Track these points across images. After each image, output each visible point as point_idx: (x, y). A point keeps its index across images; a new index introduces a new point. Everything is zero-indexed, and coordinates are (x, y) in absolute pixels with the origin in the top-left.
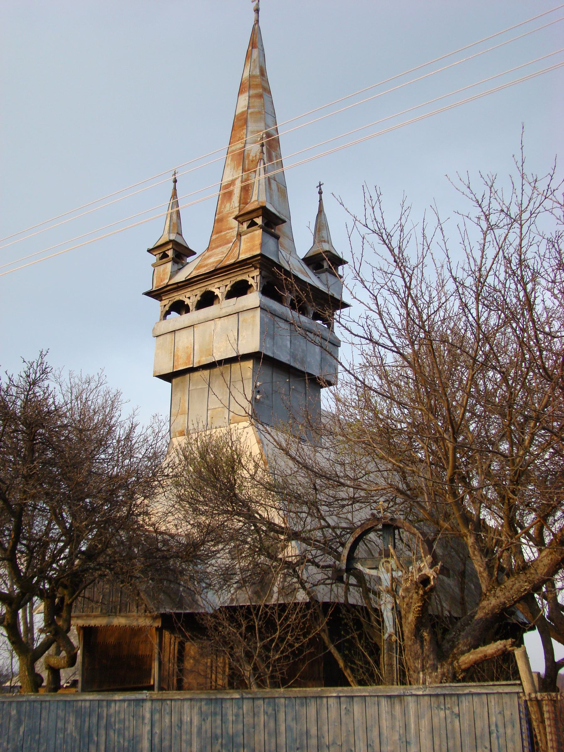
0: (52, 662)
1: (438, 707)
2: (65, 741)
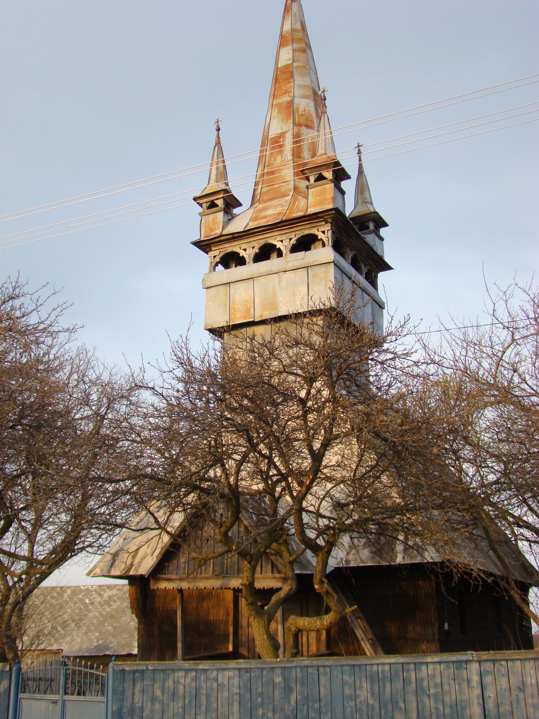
0: (301, 624)
2: (357, 710)
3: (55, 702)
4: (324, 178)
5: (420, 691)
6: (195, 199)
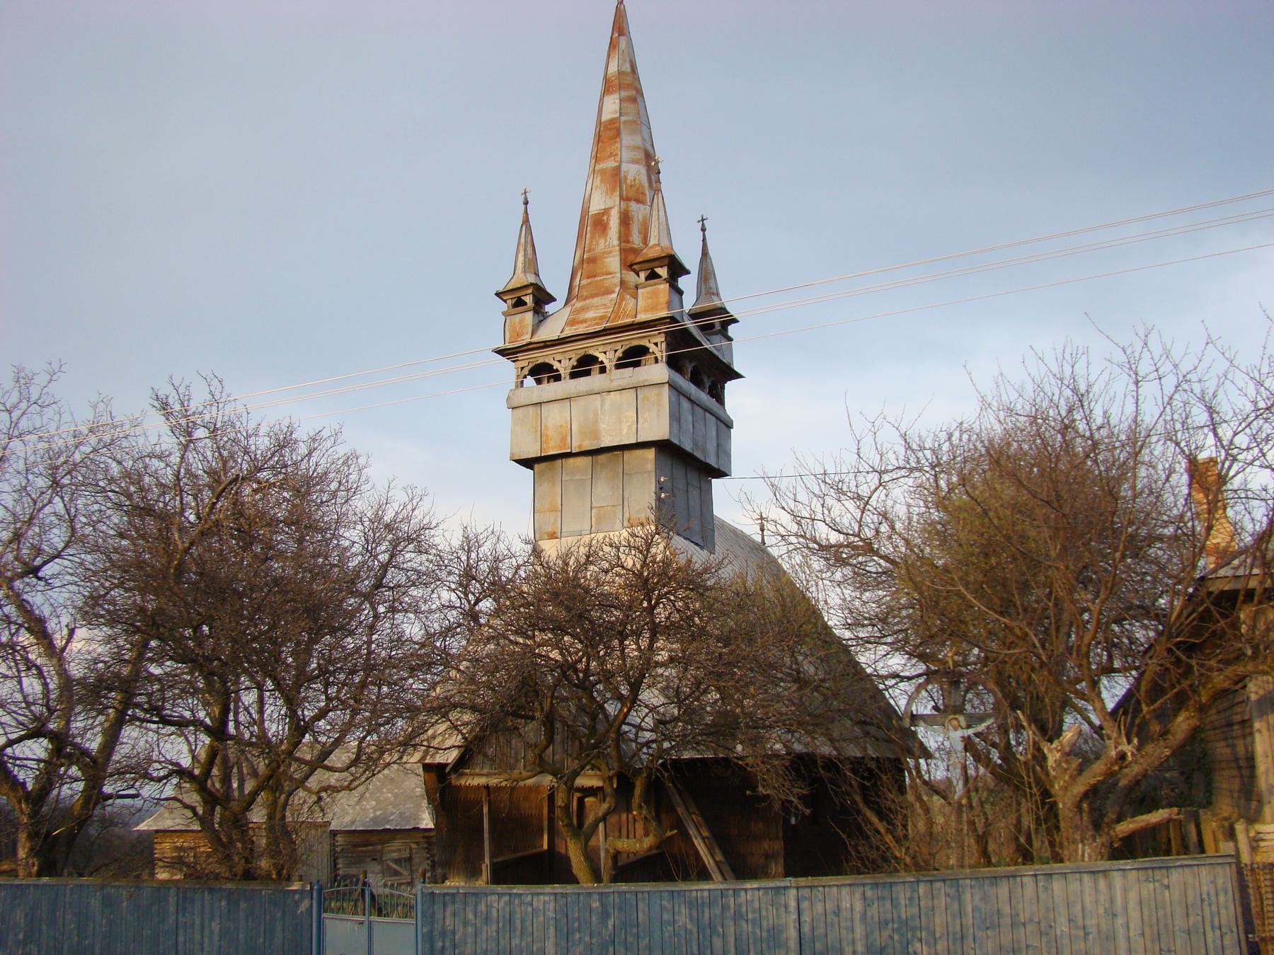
1: (1147, 880)
3: (361, 923)
4: (659, 276)
5: (738, 916)
6: (498, 294)
